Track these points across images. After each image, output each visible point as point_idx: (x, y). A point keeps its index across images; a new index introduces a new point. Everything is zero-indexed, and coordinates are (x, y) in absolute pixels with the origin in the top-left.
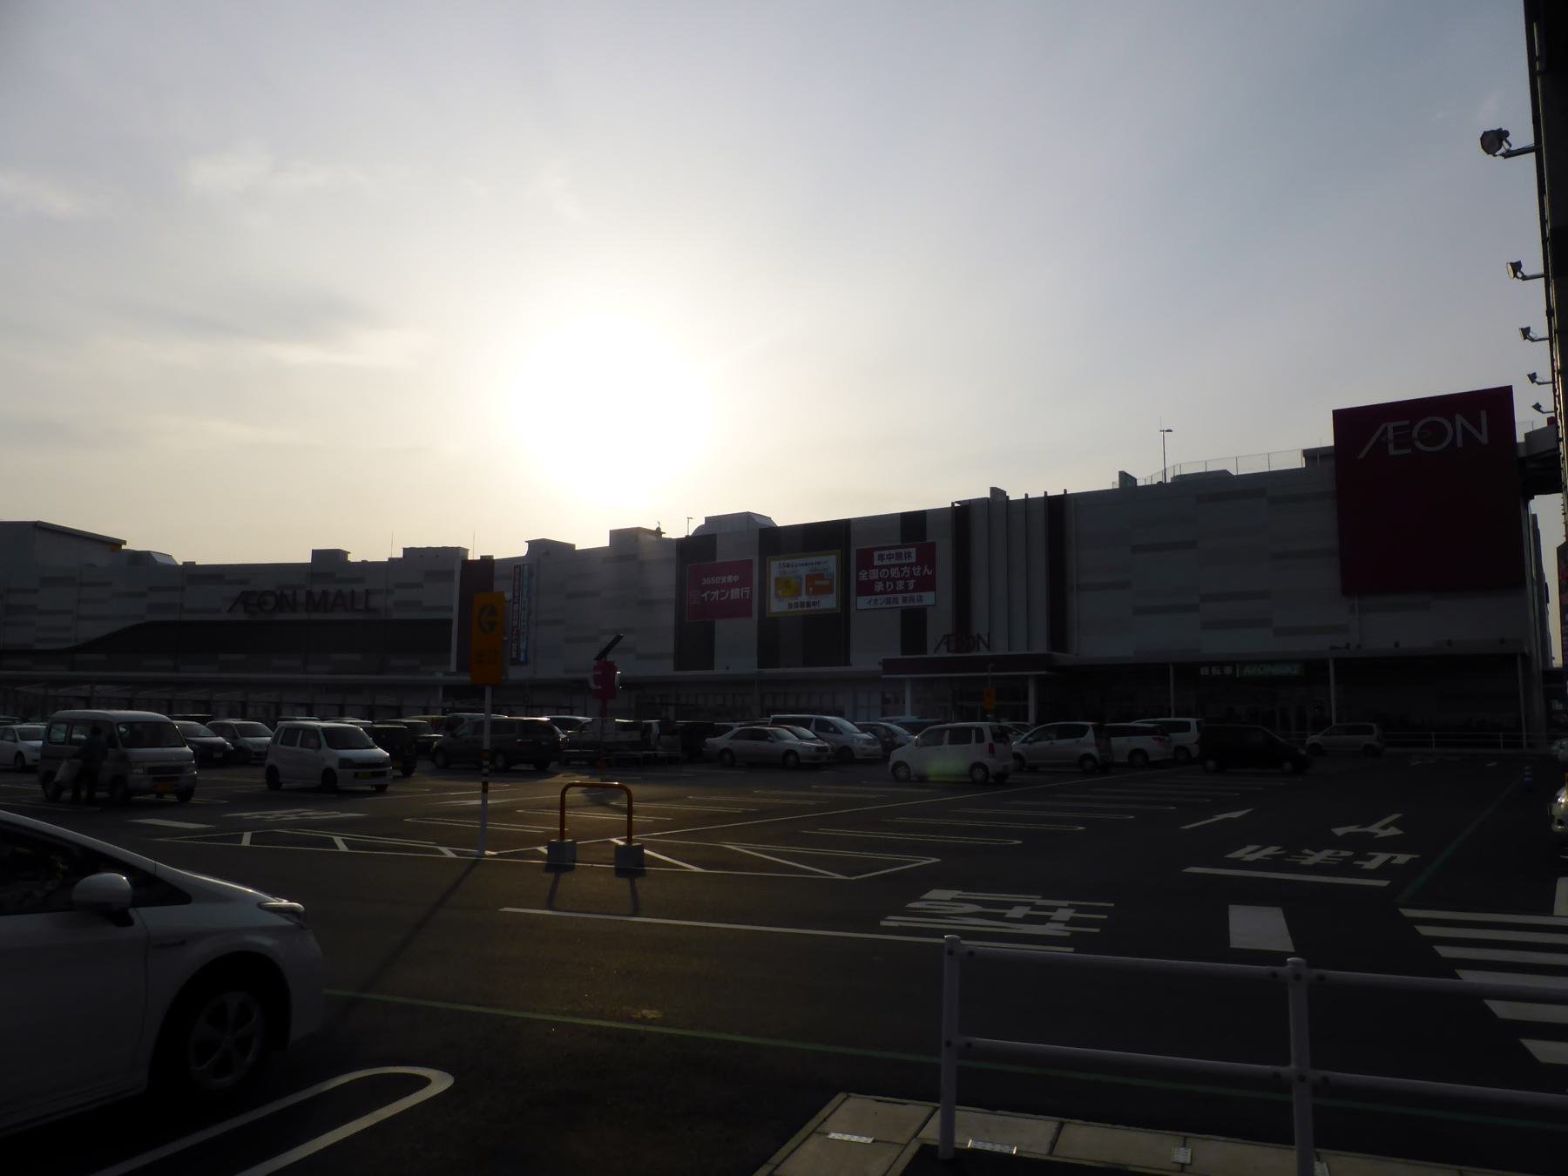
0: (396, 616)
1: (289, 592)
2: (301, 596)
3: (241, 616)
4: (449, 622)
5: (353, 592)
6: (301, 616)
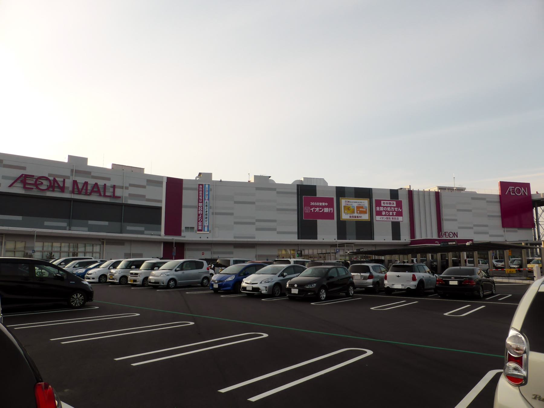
0: (130, 202)
1: (59, 180)
2: (69, 184)
3: (18, 190)
4: (160, 208)
5: (105, 185)
6: (66, 195)
